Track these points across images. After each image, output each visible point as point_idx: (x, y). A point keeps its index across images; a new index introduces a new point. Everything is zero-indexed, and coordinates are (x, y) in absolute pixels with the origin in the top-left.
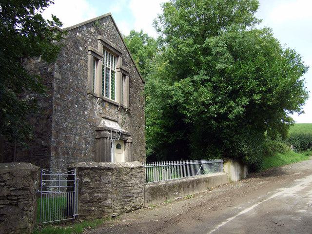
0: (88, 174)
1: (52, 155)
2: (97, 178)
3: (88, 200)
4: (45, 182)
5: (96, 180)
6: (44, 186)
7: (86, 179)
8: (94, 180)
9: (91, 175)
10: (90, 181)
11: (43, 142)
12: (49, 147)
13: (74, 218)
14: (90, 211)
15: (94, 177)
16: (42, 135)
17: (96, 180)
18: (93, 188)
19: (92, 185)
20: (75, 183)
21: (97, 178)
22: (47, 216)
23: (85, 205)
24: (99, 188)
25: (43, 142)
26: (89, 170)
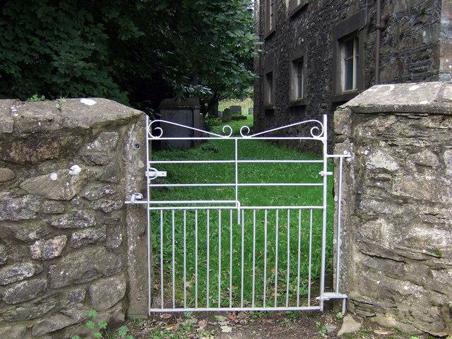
0: (387, 137)
1: (441, 68)
2: (427, 156)
3: (387, 246)
4: (159, 167)
5: (421, 167)
6: (159, 180)
7: (381, 159)
8: (411, 164)
9: (399, 140)
10: (393, 166)
11: (424, 34)
12: (434, 46)
13: (321, 308)
14: (390, 295)
15: (412, 150)
16: (423, 13)
17: (421, 167)
18: (406, 201)
19: (405, 185)
20: (325, 173)
21: (427, 156)
22: (248, 265)
23: (375, 264)
24: (432, 204)
25: (424, 34)
26: (392, 119)
